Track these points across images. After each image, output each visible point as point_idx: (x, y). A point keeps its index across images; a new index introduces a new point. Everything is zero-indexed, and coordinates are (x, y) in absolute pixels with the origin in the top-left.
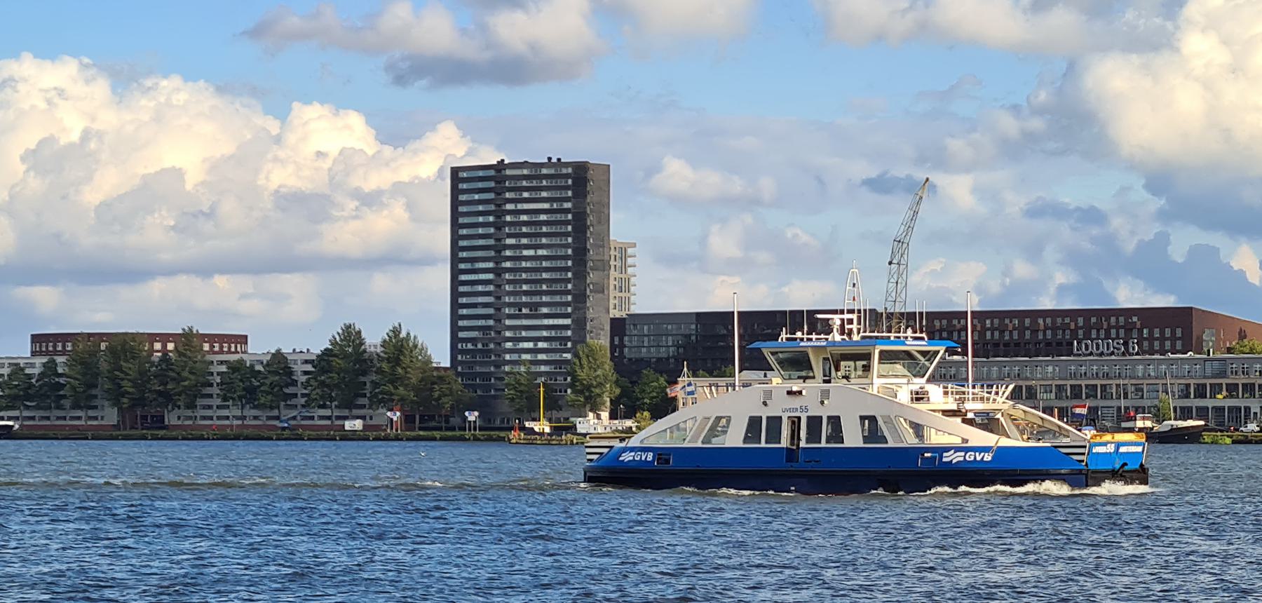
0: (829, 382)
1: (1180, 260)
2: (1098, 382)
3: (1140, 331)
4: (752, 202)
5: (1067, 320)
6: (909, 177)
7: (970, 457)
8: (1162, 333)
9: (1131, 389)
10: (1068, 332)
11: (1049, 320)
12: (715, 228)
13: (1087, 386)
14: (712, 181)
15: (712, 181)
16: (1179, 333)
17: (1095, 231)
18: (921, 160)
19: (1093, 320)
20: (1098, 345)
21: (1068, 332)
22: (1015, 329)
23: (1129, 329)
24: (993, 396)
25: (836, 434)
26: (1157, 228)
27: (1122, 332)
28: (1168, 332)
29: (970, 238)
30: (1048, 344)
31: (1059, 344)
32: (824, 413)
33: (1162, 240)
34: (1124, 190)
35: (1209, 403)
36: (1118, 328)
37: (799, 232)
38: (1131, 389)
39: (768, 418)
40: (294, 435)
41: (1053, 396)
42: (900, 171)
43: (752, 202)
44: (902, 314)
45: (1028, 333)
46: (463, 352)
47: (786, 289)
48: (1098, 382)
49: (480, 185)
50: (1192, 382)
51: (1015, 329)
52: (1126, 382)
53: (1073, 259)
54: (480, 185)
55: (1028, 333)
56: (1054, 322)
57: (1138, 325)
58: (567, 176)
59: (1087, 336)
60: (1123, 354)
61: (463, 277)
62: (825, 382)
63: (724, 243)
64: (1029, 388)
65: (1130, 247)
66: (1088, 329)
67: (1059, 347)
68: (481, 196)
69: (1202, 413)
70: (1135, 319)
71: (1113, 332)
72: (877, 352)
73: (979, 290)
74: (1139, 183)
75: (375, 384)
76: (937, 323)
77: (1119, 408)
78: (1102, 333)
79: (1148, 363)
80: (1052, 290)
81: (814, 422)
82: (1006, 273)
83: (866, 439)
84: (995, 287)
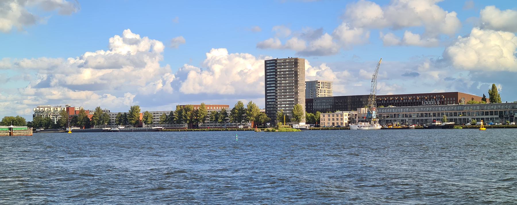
9: (437, 114)
35: (457, 117)
38: (437, 114)
46: (268, 108)
48: (428, 112)
49: (272, 65)
54: (272, 65)
58: (293, 62)
61: (268, 89)
68: (271, 67)
69: (455, 120)
75: (246, 116)
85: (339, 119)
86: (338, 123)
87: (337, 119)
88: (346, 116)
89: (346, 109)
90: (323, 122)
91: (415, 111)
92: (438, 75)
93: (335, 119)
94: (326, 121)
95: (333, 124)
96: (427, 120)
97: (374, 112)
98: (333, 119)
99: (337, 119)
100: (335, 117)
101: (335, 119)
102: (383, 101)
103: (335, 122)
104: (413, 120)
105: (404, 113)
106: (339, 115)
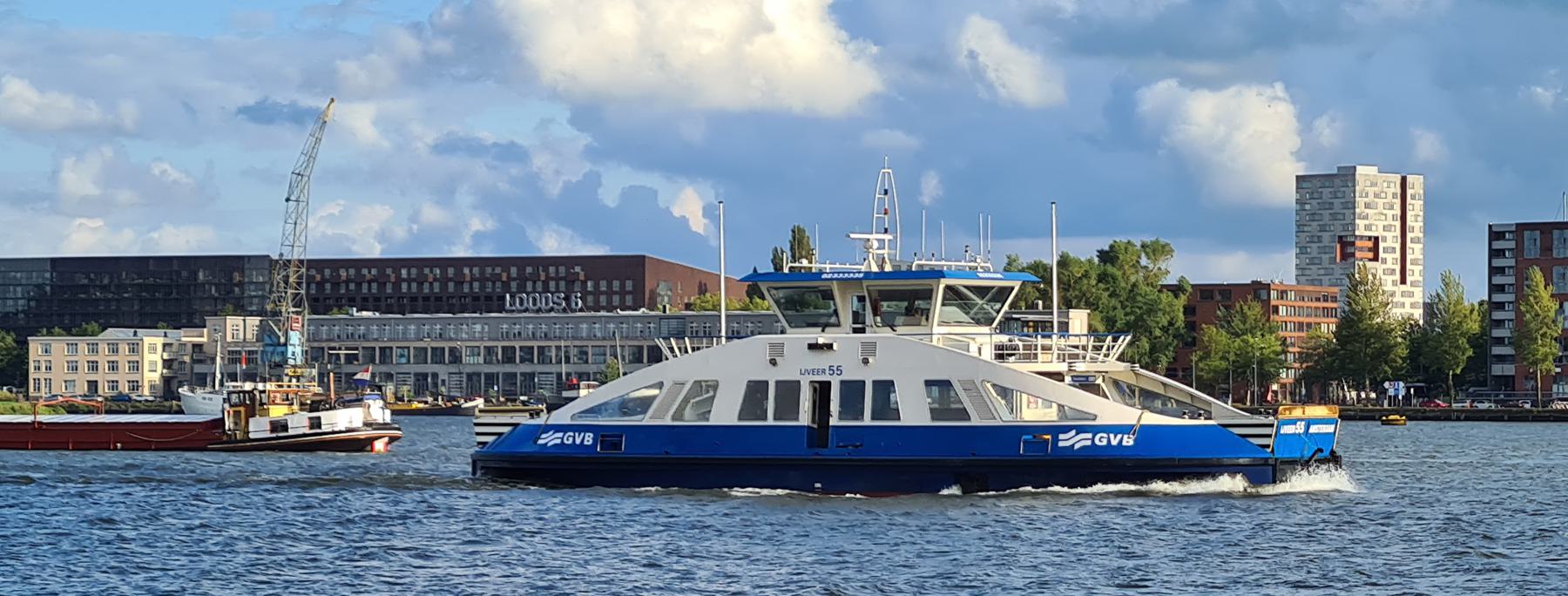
0: (863, 331)
1: (612, 205)
2: (535, 344)
3: (584, 283)
4: (115, 131)
5: (498, 270)
6: (293, 104)
7: (1101, 440)
8: (610, 285)
9: (573, 352)
10: (498, 284)
11: (476, 270)
12: (69, 162)
13: (521, 348)
14: (62, 107)
15: (62, 107)
16: (629, 285)
17: (515, 170)
18: (308, 85)
19: (529, 270)
20: (521, 300)
21: (498, 284)
22: (435, 280)
23: (571, 281)
24: (1101, 358)
25: (884, 407)
26: (588, 167)
27: (562, 284)
28: (603, 286)
29: (374, 177)
30: (476, 298)
31: (489, 298)
32: (869, 376)
33: (592, 182)
34: (545, 123)
36: (557, 279)
37: (166, 166)
38: (573, 352)
39: (777, 382)
40: (1446, 416)
41: (481, 360)
42: (282, 98)
43: (115, 131)
44: (301, 261)
45: (451, 286)
47: (155, 235)
48: (535, 344)
50: (517, 344)
51: (435, 280)
52: (568, 343)
53: (489, 201)
55: (451, 286)
56: (482, 272)
57: (582, 277)
59: (522, 289)
60: (564, 310)
62: (855, 331)
63: (78, 179)
64: (452, 350)
65: (555, 190)
66: (522, 280)
67: (493, 303)
70: (578, 269)
71: (552, 284)
72: (941, 287)
73: (382, 237)
74: (562, 114)
76: (343, 273)
77: (559, 375)
78: (539, 286)
79: (594, 320)
80: (468, 239)
81: (852, 391)
82: (414, 218)
83: (935, 414)
84: (400, 233)
85: (124, 367)
86: (114, 384)
87: (114, 366)
88: (152, 352)
89: (148, 320)
90: (42, 375)
91: (472, 333)
92: (375, 123)
93: (104, 366)
94: (59, 375)
95: (93, 385)
96: (532, 375)
97: (295, 337)
98: (94, 366)
99: (114, 366)
100: (103, 357)
101: (104, 366)
102: (334, 285)
103: (103, 377)
104: (469, 376)
105: (428, 344)
106: (124, 348)
